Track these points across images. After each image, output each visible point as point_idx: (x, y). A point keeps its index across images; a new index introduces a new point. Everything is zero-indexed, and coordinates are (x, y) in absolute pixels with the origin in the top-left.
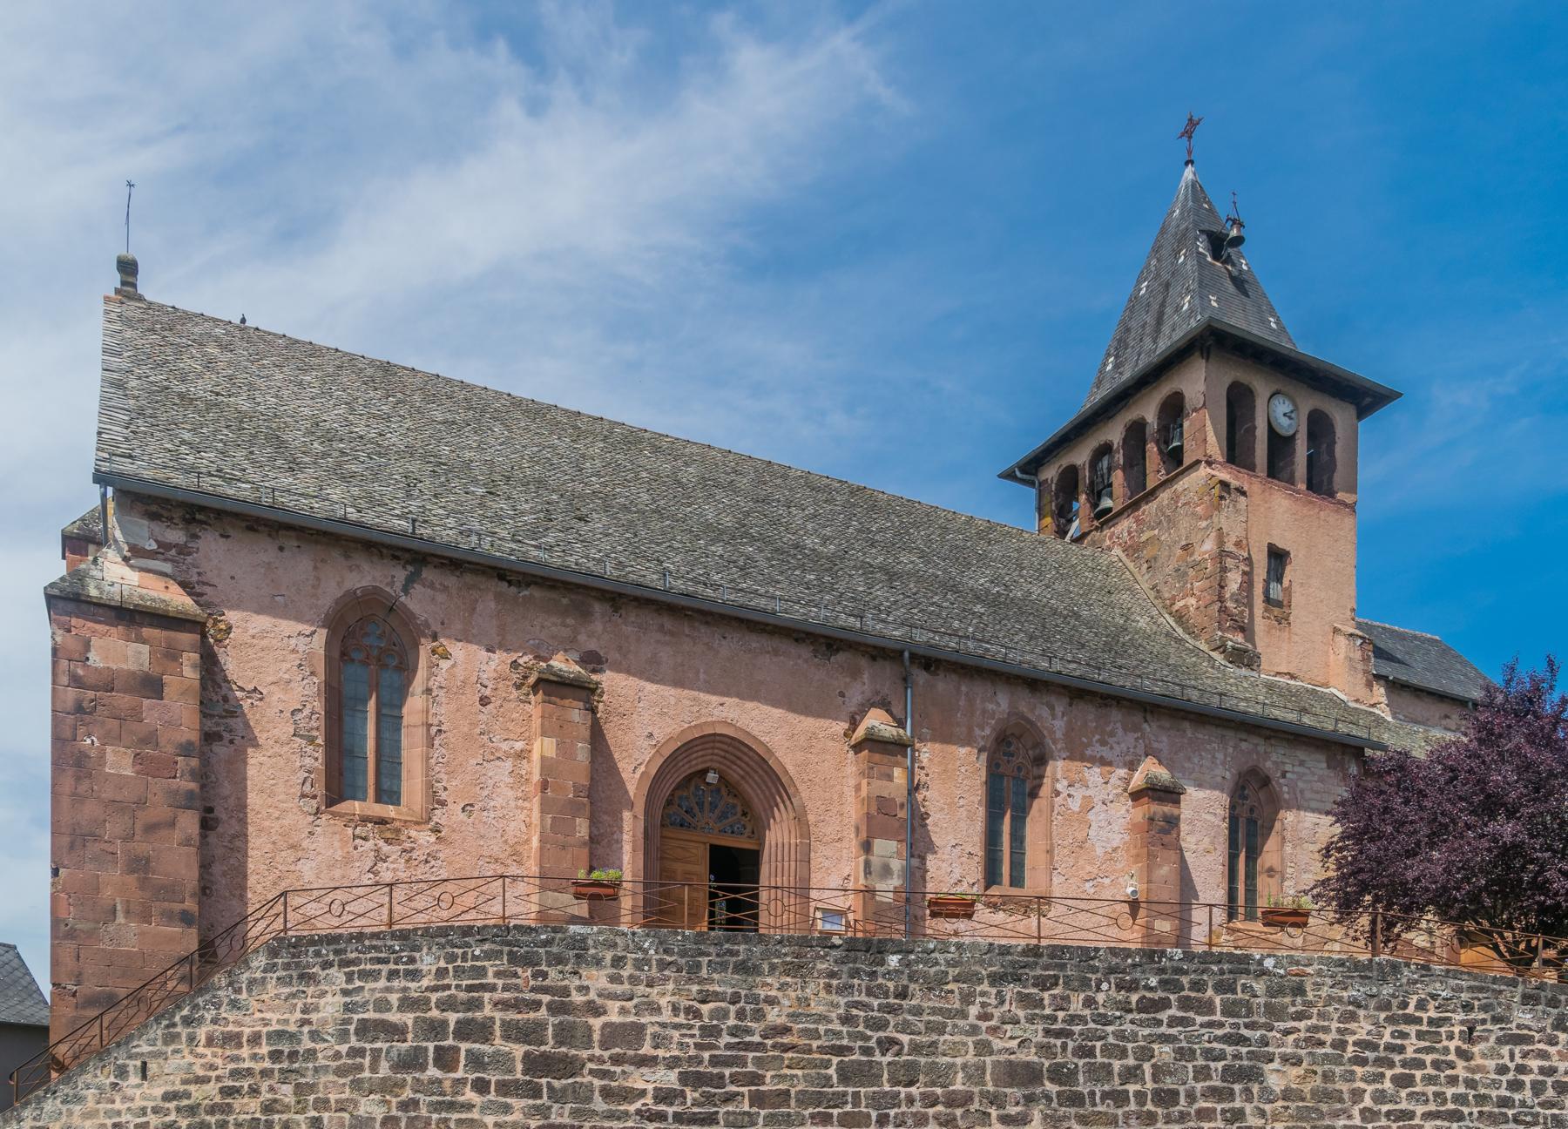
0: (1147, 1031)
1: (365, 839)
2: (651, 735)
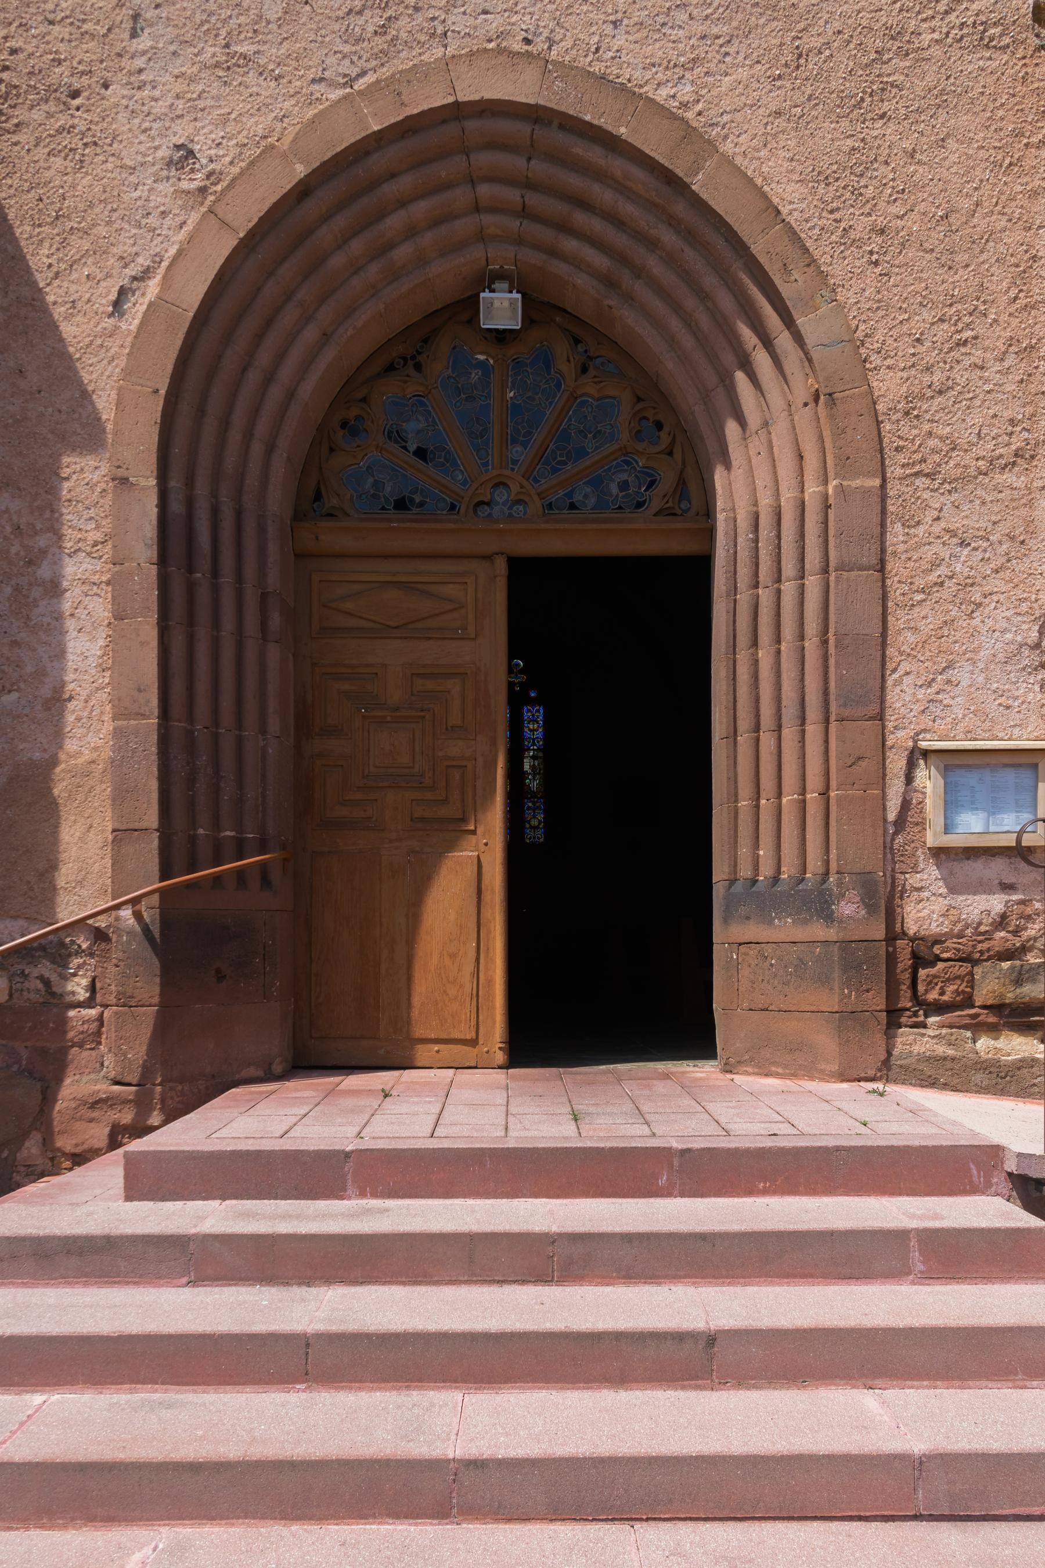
2: (185, 155)
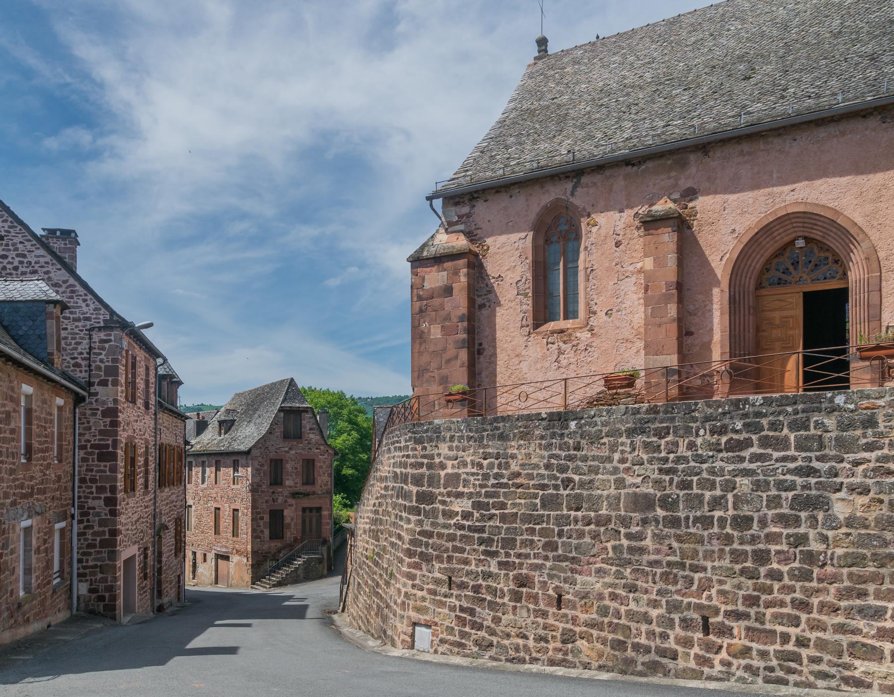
0: (731, 467)
1: (553, 343)
